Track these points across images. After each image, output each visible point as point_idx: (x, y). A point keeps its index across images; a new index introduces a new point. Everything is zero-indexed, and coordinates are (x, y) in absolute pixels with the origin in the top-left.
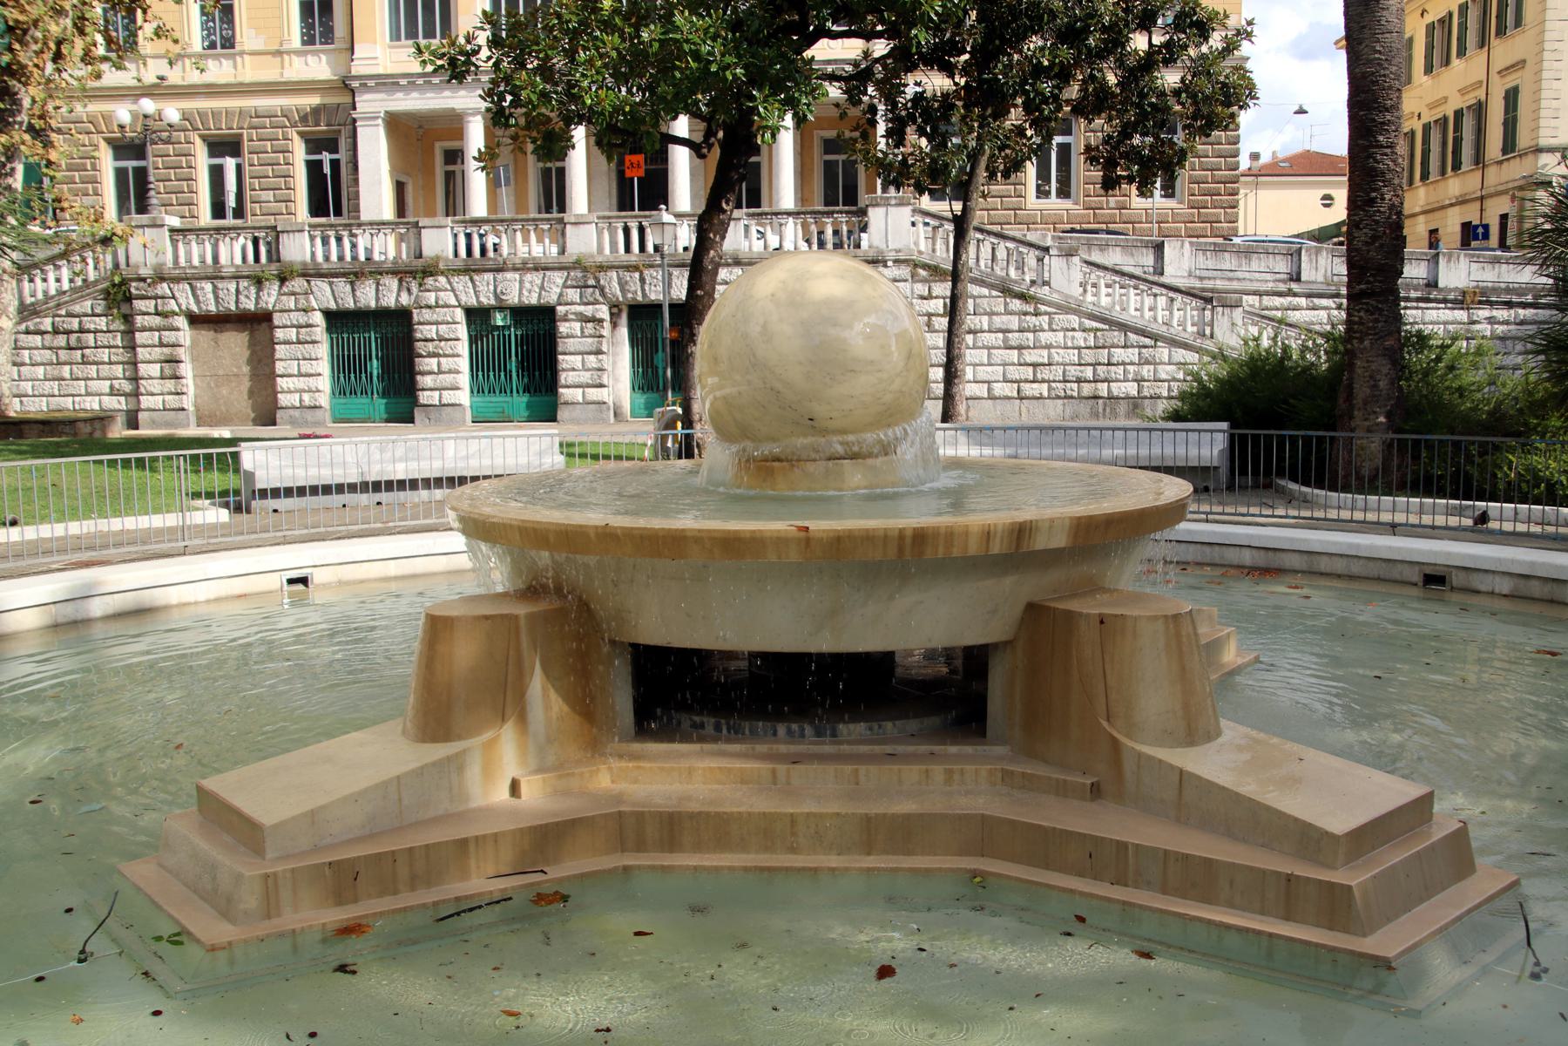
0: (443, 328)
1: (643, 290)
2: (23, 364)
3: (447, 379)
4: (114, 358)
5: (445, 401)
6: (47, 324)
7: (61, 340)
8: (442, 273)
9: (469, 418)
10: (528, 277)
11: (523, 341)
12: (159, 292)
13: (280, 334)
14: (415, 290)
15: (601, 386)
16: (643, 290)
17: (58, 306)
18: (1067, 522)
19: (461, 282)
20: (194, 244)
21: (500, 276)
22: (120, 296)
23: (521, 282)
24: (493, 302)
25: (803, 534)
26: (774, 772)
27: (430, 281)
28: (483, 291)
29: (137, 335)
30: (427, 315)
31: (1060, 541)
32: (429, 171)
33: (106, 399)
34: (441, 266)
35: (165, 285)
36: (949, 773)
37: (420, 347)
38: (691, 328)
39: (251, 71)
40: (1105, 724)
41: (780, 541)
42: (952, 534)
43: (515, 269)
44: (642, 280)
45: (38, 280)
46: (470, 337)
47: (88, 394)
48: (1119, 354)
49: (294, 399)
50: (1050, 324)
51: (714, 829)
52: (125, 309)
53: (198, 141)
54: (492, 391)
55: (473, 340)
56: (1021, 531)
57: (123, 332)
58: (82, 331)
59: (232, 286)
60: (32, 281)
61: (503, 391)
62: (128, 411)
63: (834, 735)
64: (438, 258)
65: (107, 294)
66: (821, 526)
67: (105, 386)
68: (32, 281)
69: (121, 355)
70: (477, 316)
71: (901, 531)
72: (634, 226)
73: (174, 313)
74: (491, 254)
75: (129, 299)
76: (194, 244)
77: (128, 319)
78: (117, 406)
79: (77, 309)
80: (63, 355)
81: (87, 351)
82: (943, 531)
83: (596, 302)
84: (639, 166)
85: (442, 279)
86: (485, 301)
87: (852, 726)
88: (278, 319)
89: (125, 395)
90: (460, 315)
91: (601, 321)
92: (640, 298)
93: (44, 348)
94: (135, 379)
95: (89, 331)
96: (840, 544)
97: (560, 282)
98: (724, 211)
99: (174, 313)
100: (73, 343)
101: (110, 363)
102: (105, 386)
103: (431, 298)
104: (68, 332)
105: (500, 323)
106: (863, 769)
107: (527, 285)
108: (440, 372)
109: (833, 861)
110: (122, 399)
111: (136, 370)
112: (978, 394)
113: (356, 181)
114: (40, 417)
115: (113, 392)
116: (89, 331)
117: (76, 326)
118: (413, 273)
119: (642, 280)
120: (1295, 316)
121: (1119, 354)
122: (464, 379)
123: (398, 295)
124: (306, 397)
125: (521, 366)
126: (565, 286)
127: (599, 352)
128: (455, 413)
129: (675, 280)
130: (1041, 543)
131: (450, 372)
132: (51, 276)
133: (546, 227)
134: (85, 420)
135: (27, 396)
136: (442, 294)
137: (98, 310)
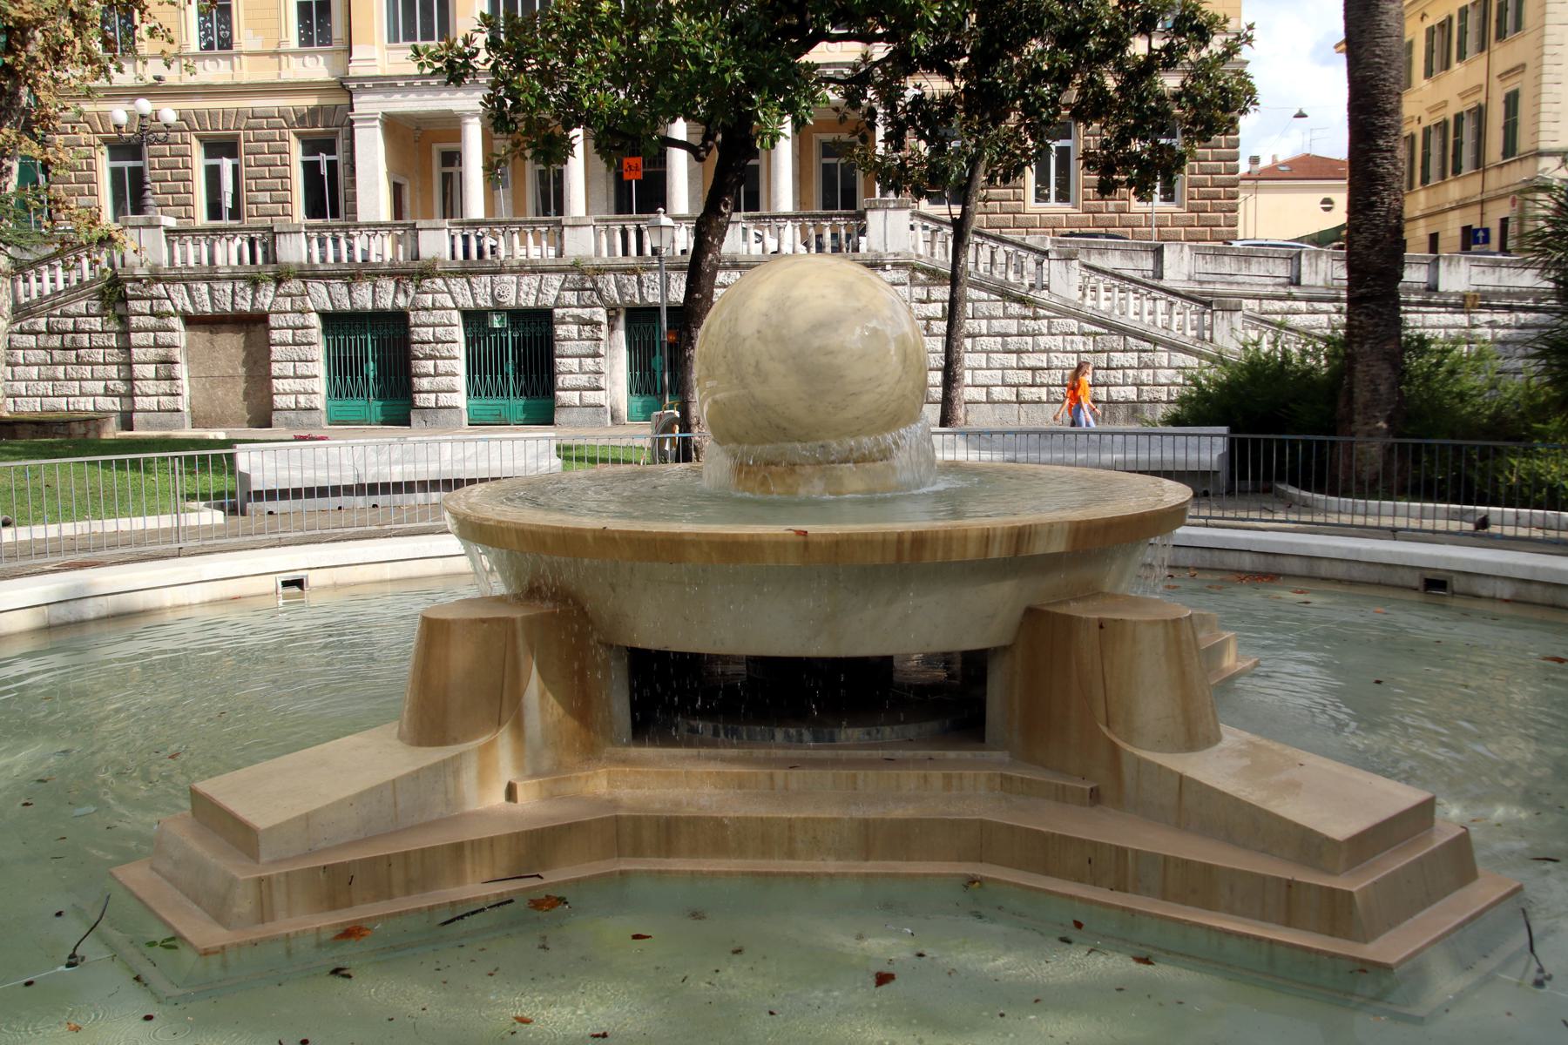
0: (439, 330)
1: (641, 293)
2: (17, 364)
3: (444, 382)
4: (108, 359)
5: (441, 404)
6: (41, 324)
7: (56, 340)
8: (439, 275)
9: (324, 418)
10: (526, 280)
11: (518, 344)
12: (155, 292)
13: (276, 335)
14: (412, 292)
15: (599, 389)
16: (641, 293)
17: (53, 306)
18: (1066, 527)
19: (458, 285)
20: (190, 244)
21: (497, 279)
22: (115, 297)
23: (519, 284)
24: (490, 304)
25: (801, 538)
26: (771, 777)
27: (427, 283)
28: (480, 293)
29: (133, 335)
30: (424, 317)
31: (1058, 546)
32: (426, 173)
33: (100, 400)
34: (438, 268)
35: (161, 286)
36: (948, 778)
37: (417, 349)
38: (689, 332)
39: (248, 72)
40: (1104, 729)
41: (778, 545)
42: (951, 538)
43: (513, 272)
44: (640, 283)
45: (33, 280)
46: (467, 339)
47: (82, 394)
48: (1118, 359)
49: (289, 401)
50: (1049, 328)
51: (710, 834)
52: (120, 309)
53: (195, 142)
54: (488, 394)
55: (469, 343)
56: (1021, 535)
57: (118, 333)
58: (76, 331)
59: (228, 287)
60: (26, 280)
61: (500, 393)
62: (122, 412)
63: (832, 740)
64: (435, 260)
65: (102, 293)
66: (813, 529)
67: (99, 387)
68: (26, 280)
69: (115, 355)
70: (474, 319)
71: (900, 535)
72: (631, 228)
73: (170, 314)
74: (488, 256)
75: (124, 299)
76: (190, 244)
77: (123, 319)
78: (112, 407)
79: (72, 309)
80: (58, 355)
81: (82, 352)
82: (941, 535)
83: (593, 305)
84: (637, 169)
85: (439, 282)
86: (481, 303)
87: (850, 731)
88: (274, 321)
89: (120, 396)
90: (456, 317)
91: (599, 324)
92: (637, 301)
93: (38, 348)
94: (130, 380)
95: (83, 332)
96: (838, 545)
97: (557, 284)
98: (723, 215)
99: (170, 314)
100: (68, 342)
101: (105, 364)
102: (99, 387)
103: (428, 300)
104: (63, 333)
105: (497, 325)
106: (861, 774)
107: (525, 288)
108: (437, 375)
109: (832, 865)
110: (117, 400)
111: (131, 371)
112: (977, 398)
113: (353, 182)
114: (34, 417)
115: (107, 393)
116: (83, 332)
117: (71, 327)
118: (410, 275)
119: (640, 283)
120: (1295, 320)
121: (1118, 359)
122: (461, 382)
123: (395, 297)
124: (302, 399)
125: (518, 368)
126: (562, 289)
127: (596, 355)
128: (453, 416)
129: (672, 283)
130: (1040, 548)
131: (447, 374)
132: (46, 277)
133: (544, 229)
134: (80, 421)
135: (20, 396)
136: (438, 296)
137: (93, 310)
